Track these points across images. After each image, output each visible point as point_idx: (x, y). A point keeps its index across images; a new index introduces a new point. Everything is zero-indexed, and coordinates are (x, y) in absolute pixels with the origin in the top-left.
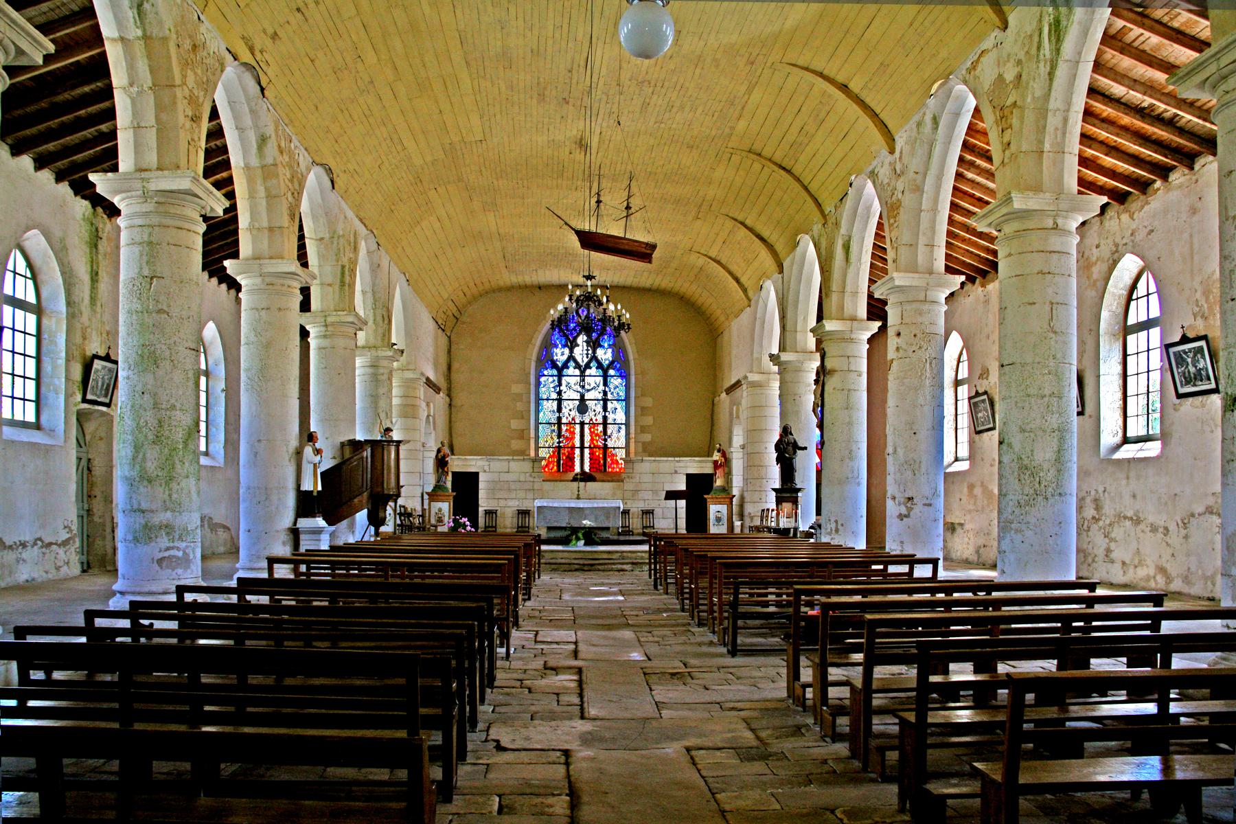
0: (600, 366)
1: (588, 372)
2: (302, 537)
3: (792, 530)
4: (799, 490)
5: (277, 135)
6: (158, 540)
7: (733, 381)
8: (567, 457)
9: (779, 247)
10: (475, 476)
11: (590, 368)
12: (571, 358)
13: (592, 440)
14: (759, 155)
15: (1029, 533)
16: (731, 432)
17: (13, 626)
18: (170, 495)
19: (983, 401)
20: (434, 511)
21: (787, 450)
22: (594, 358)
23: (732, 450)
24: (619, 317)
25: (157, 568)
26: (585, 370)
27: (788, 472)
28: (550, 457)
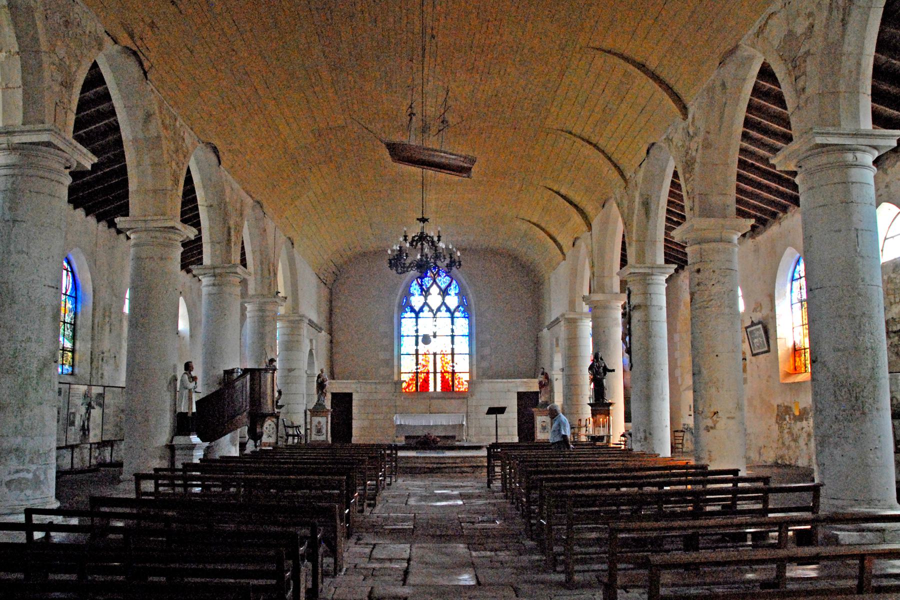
0: (448, 310)
1: (439, 314)
2: (177, 452)
3: (605, 438)
4: (610, 404)
5: (161, 112)
6: (9, 463)
7: (553, 319)
8: (423, 380)
9: (589, 209)
10: (350, 395)
11: (441, 311)
12: (426, 304)
13: (443, 367)
14: (570, 133)
15: (847, 447)
16: (552, 357)
17: (23, 509)
18: (22, 421)
19: (758, 330)
20: (315, 423)
21: (599, 372)
22: (444, 303)
23: (553, 373)
24: (451, 255)
25: (6, 490)
26: (436, 312)
27: (599, 391)
28: (410, 380)
